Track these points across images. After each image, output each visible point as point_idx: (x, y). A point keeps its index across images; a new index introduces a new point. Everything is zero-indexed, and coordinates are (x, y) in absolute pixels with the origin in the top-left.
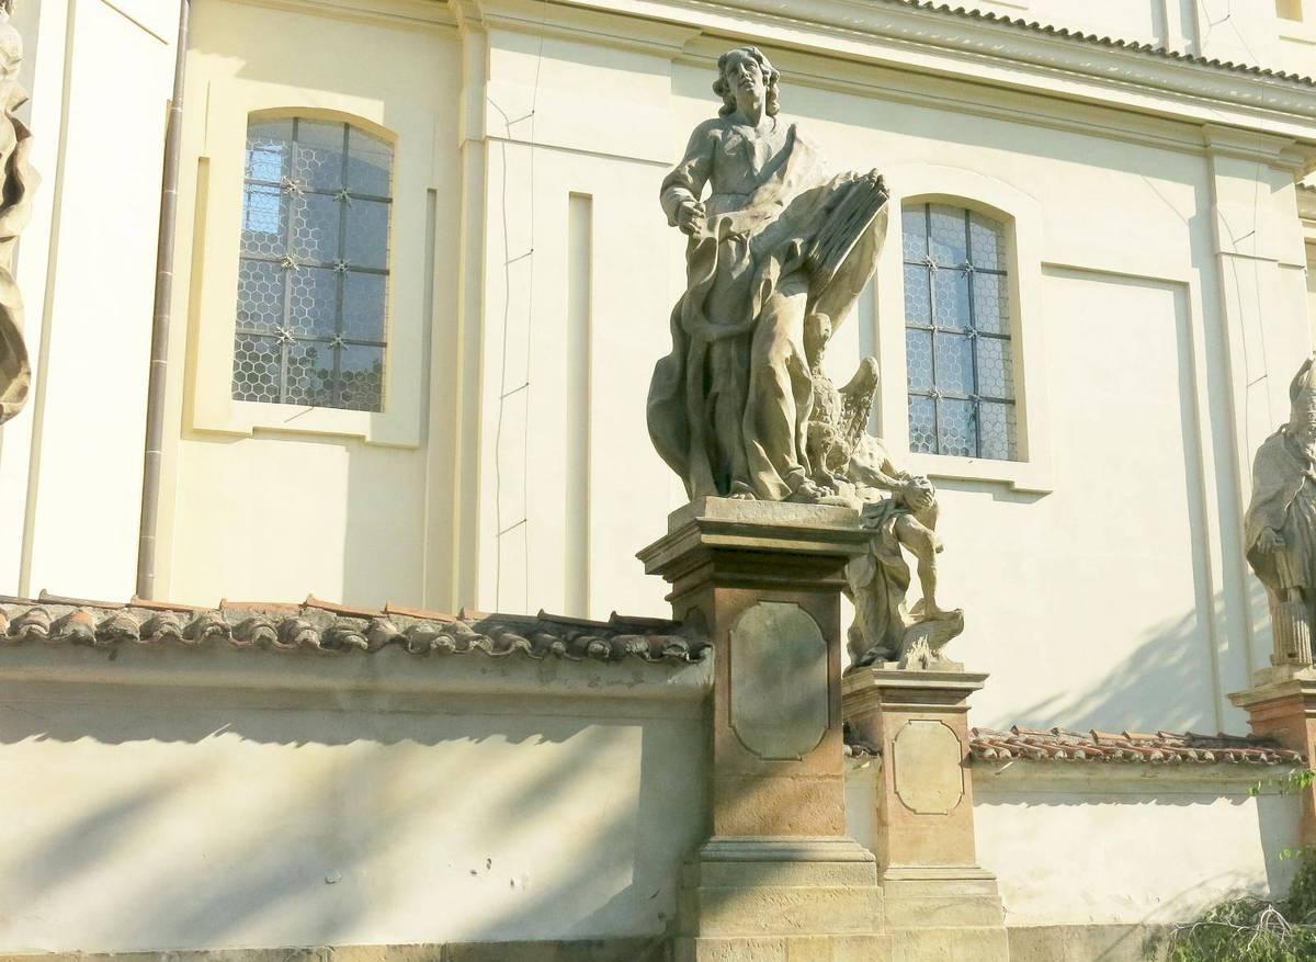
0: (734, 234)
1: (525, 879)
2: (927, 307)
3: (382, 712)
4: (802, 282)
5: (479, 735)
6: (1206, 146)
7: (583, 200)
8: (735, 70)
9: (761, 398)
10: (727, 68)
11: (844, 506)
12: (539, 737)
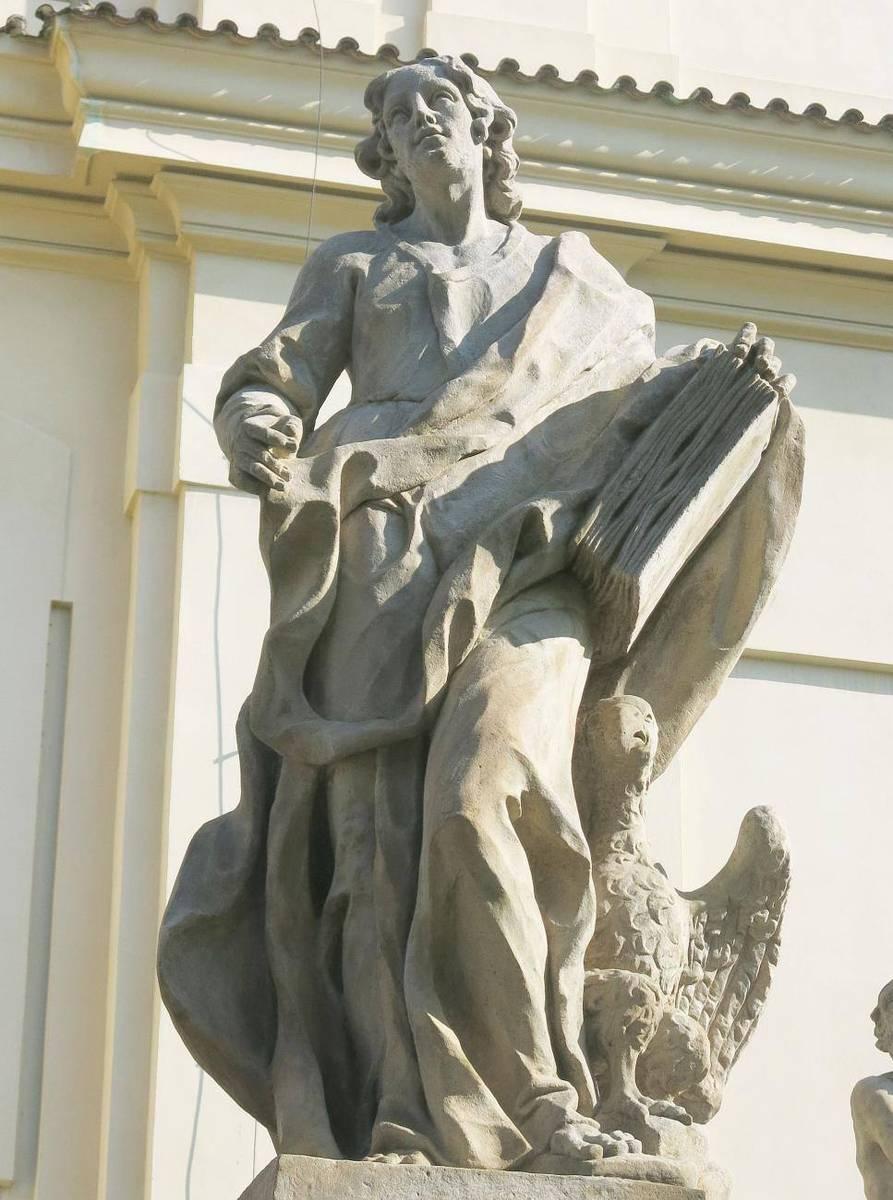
0: (382, 492)
4: (566, 610)
8: (405, 109)
9: (448, 903)
10: (386, 108)
11: (664, 1180)
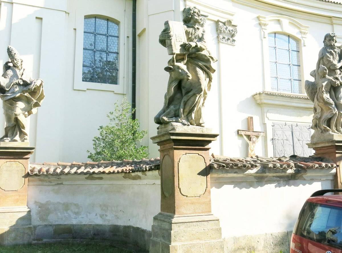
6: (332, 22)
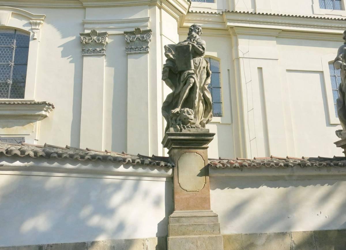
1: (328, 216)
2: (336, 85)
3: (294, 180)
5: (315, 184)
7: (260, 69)
12: (327, 184)
